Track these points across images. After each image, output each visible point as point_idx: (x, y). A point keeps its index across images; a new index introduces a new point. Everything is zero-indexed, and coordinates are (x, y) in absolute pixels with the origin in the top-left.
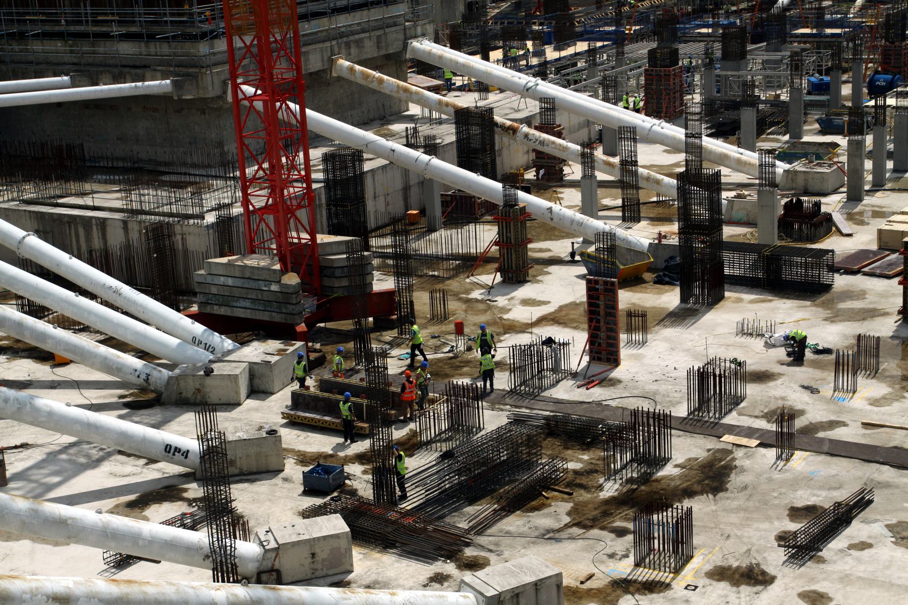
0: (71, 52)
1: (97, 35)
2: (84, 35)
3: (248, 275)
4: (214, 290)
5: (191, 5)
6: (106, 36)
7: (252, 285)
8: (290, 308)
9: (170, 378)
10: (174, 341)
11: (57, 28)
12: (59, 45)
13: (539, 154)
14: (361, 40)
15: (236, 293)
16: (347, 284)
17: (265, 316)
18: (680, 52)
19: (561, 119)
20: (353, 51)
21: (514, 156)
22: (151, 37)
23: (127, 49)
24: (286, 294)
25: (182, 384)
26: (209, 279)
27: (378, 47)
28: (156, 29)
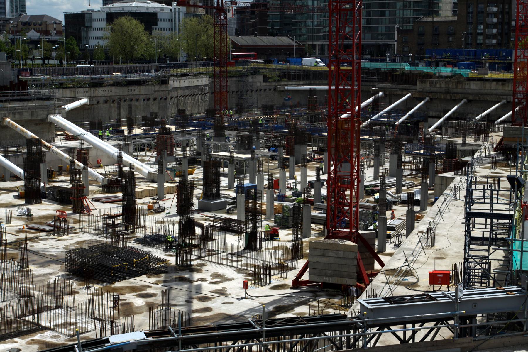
14: (22, 112)
27: (32, 116)
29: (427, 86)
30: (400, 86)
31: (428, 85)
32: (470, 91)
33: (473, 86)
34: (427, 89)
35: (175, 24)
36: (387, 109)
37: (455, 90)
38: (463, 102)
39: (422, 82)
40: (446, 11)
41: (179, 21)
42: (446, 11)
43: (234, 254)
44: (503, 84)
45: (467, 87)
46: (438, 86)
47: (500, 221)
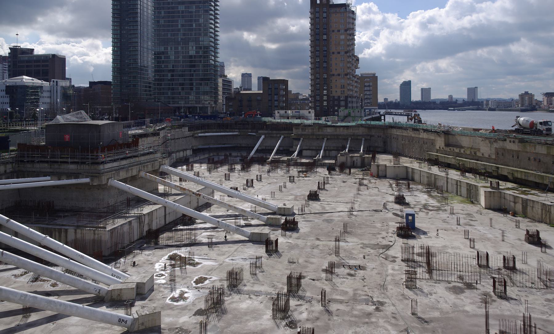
2: (57, 162)
5: (97, 152)
6: (67, 163)
10: (179, 228)
11: (46, 159)
16: (545, 153)
18: (5, 92)
20: (145, 168)
22: (84, 163)
23: (72, 167)
28: (84, 161)
29: (300, 132)
30: (275, 132)
31: (301, 130)
32: (327, 133)
33: (329, 130)
34: (299, 133)
35: (54, 94)
37: (318, 133)
38: (281, 138)
39: (296, 129)
40: (318, 2)
41: (57, 92)
42: (318, 2)
43: (96, 176)
44: (347, 129)
45: (325, 131)
46: (307, 131)
47: (5, 252)
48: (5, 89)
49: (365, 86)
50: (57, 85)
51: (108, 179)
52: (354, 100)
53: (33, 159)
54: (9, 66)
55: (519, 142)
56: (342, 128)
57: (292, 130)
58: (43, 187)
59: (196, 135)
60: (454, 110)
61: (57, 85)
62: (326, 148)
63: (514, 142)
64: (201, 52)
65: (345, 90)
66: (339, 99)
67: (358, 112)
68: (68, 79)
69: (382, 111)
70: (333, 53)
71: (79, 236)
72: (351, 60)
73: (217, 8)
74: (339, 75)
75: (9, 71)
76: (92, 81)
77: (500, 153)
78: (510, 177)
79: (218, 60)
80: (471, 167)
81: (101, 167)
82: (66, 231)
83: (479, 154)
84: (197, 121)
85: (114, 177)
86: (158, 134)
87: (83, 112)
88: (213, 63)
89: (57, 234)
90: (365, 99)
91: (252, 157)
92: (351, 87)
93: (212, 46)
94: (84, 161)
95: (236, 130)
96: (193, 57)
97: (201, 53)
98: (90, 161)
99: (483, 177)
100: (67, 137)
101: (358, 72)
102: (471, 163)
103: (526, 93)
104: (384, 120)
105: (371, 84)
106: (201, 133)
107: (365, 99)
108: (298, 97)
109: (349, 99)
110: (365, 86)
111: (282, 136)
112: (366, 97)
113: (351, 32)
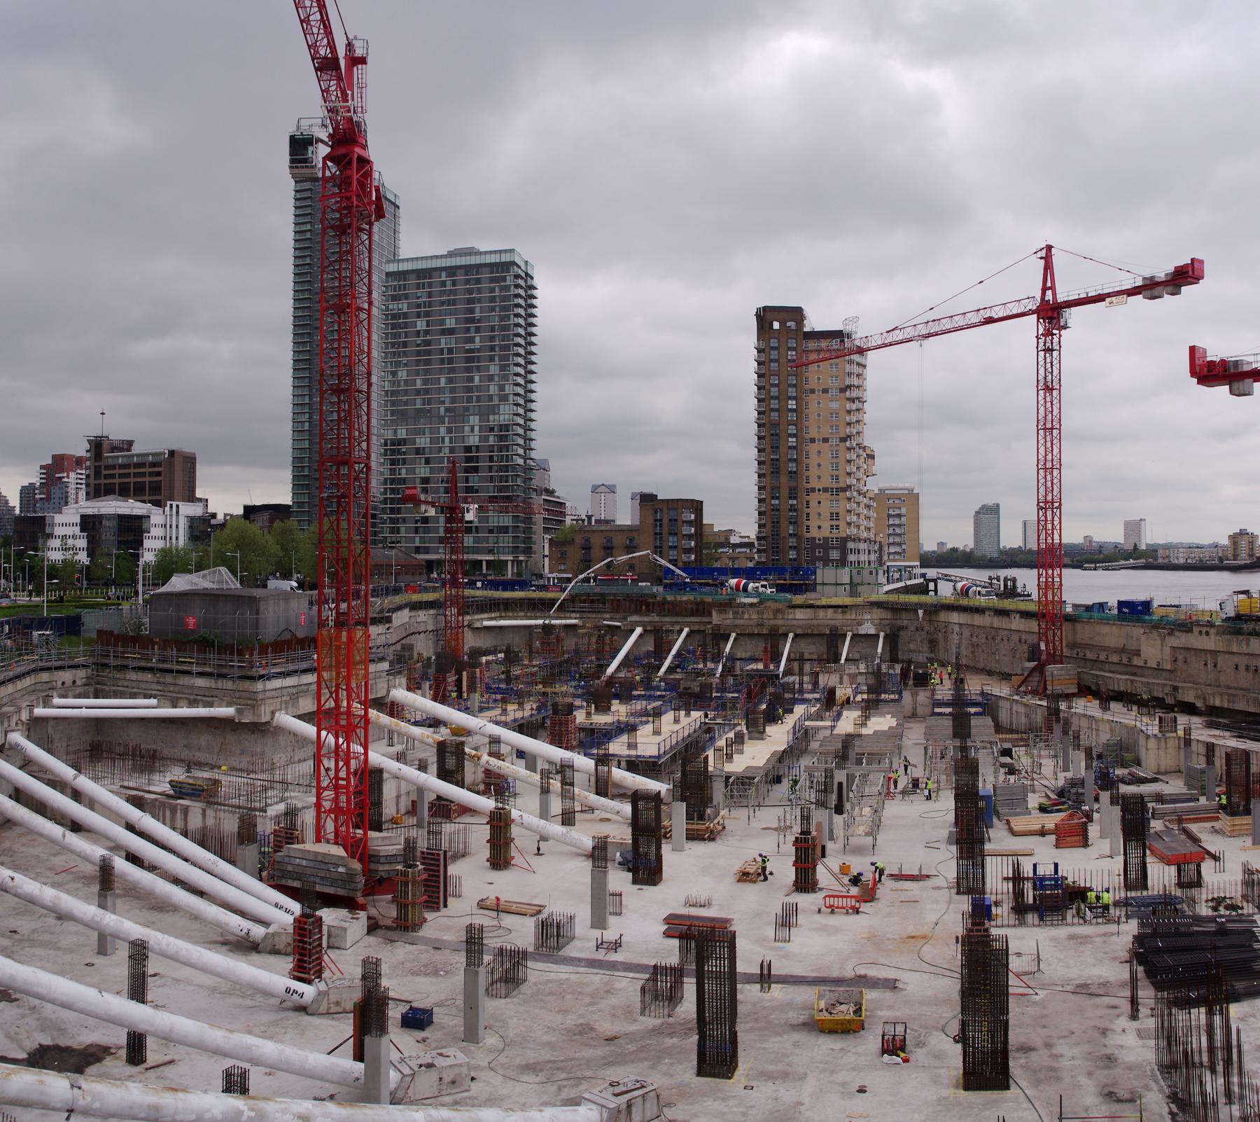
0: (158, 682)
1: (179, 672)
2: (171, 671)
3: (320, 858)
4: (290, 868)
6: (189, 673)
7: (324, 867)
8: (353, 885)
9: (267, 934)
12: (149, 676)
13: (488, 772)
15: (308, 871)
17: (331, 890)
19: (504, 749)
21: (471, 773)
22: (224, 676)
24: (351, 875)
25: (276, 939)
26: (287, 860)
30: (667, 619)
33: (800, 614)
36: (674, 651)
39: (720, 612)
46: (746, 616)
48: (78, 520)
49: (889, 516)
50: (178, 512)
51: (273, 713)
52: (862, 546)
53: (125, 663)
54: (88, 476)
55: (1217, 634)
56: (830, 611)
57: (710, 615)
58: (143, 719)
59: (478, 625)
60: (1095, 569)
61: (178, 512)
62: (792, 656)
63: (1207, 633)
64: (491, 439)
65: (842, 524)
66: (826, 544)
67: (871, 573)
68: (200, 500)
69: (932, 573)
70: (813, 440)
71: (210, 822)
72: (854, 457)
73: (533, 367)
74: (826, 490)
75: (87, 485)
76: (249, 503)
77: (1180, 658)
78: (1199, 704)
79: (533, 454)
80: (1122, 689)
81: (259, 686)
82: (186, 810)
83: (1137, 661)
84: (479, 593)
85: (287, 708)
86: (389, 620)
87: (223, 569)
88: (521, 461)
89: (168, 813)
90: (889, 545)
91: (611, 677)
92: (855, 518)
93: (519, 425)
94: (224, 671)
95: (573, 615)
96: (474, 449)
97: (492, 441)
98: (237, 673)
99: (1145, 710)
100: (191, 621)
101: (873, 486)
102: (1120, 681)
103: (1242, 533)
104: (936, 591)
105: (903, 511)
106: (491, 619)
107: (889, 545)
108: (727, 539)
109: (851, 545)
110: (889, 516)
111: (686, 630)
112: (891, 540)
113: (855, 394)
